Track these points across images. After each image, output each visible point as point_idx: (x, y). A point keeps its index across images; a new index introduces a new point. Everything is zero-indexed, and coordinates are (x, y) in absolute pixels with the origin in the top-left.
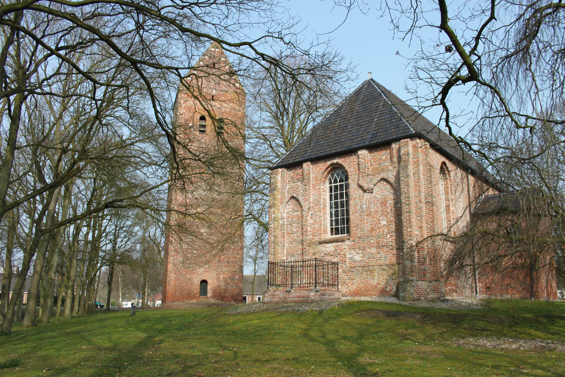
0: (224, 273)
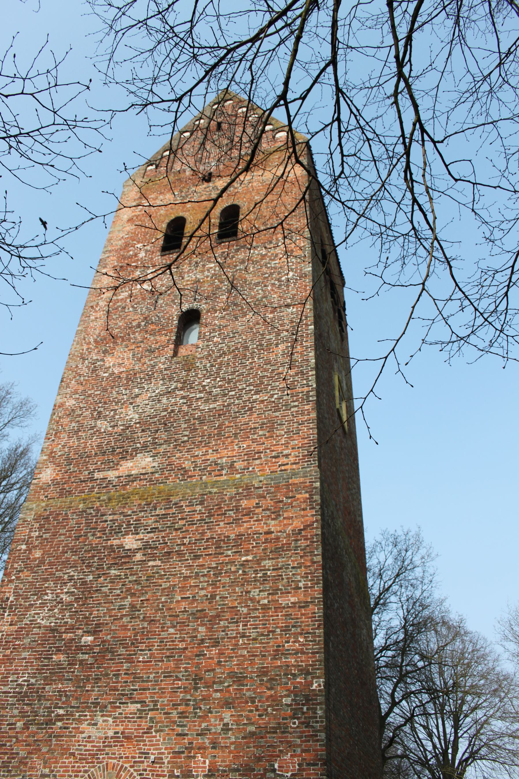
0: (215, 745)
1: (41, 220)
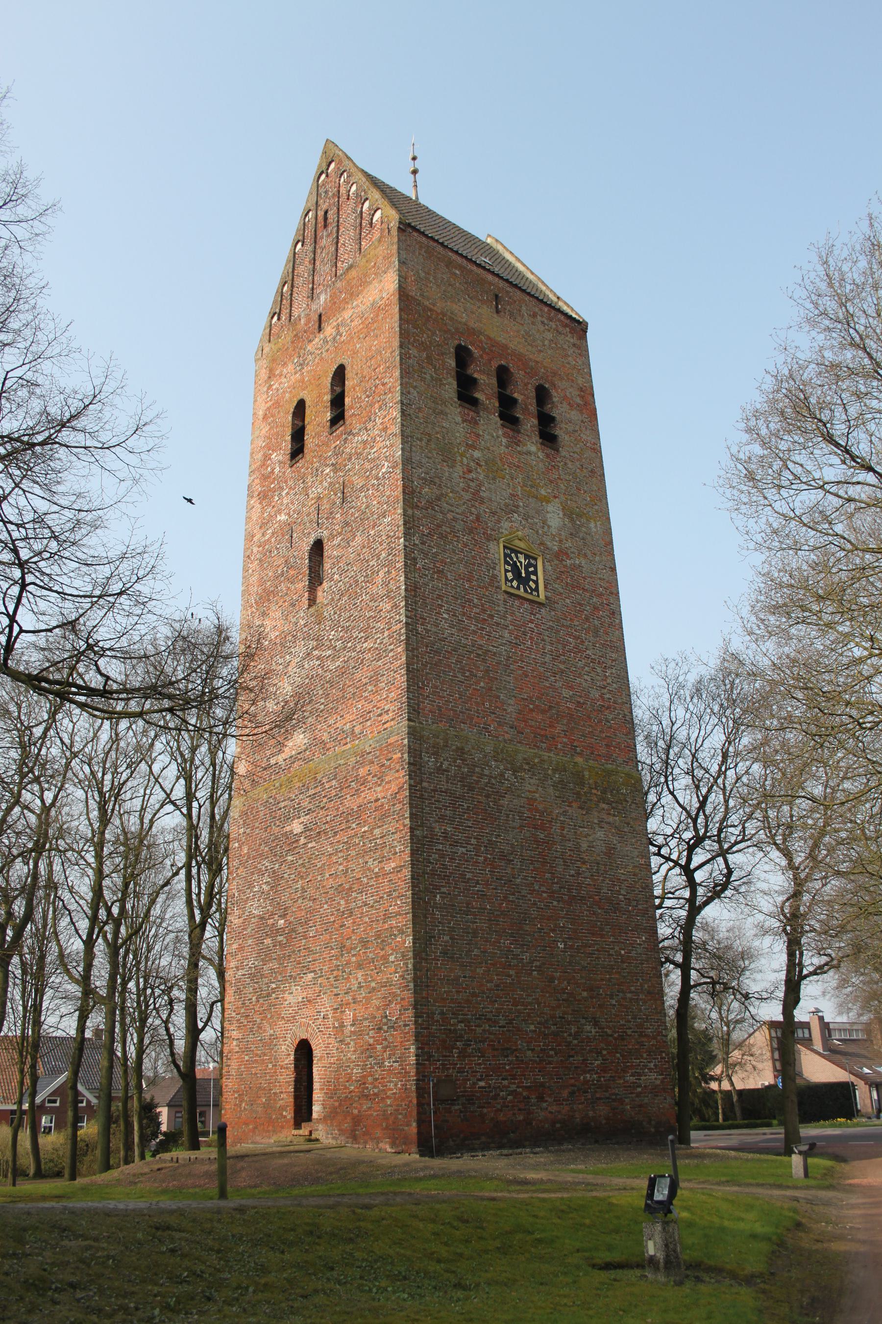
1: (340, 374)
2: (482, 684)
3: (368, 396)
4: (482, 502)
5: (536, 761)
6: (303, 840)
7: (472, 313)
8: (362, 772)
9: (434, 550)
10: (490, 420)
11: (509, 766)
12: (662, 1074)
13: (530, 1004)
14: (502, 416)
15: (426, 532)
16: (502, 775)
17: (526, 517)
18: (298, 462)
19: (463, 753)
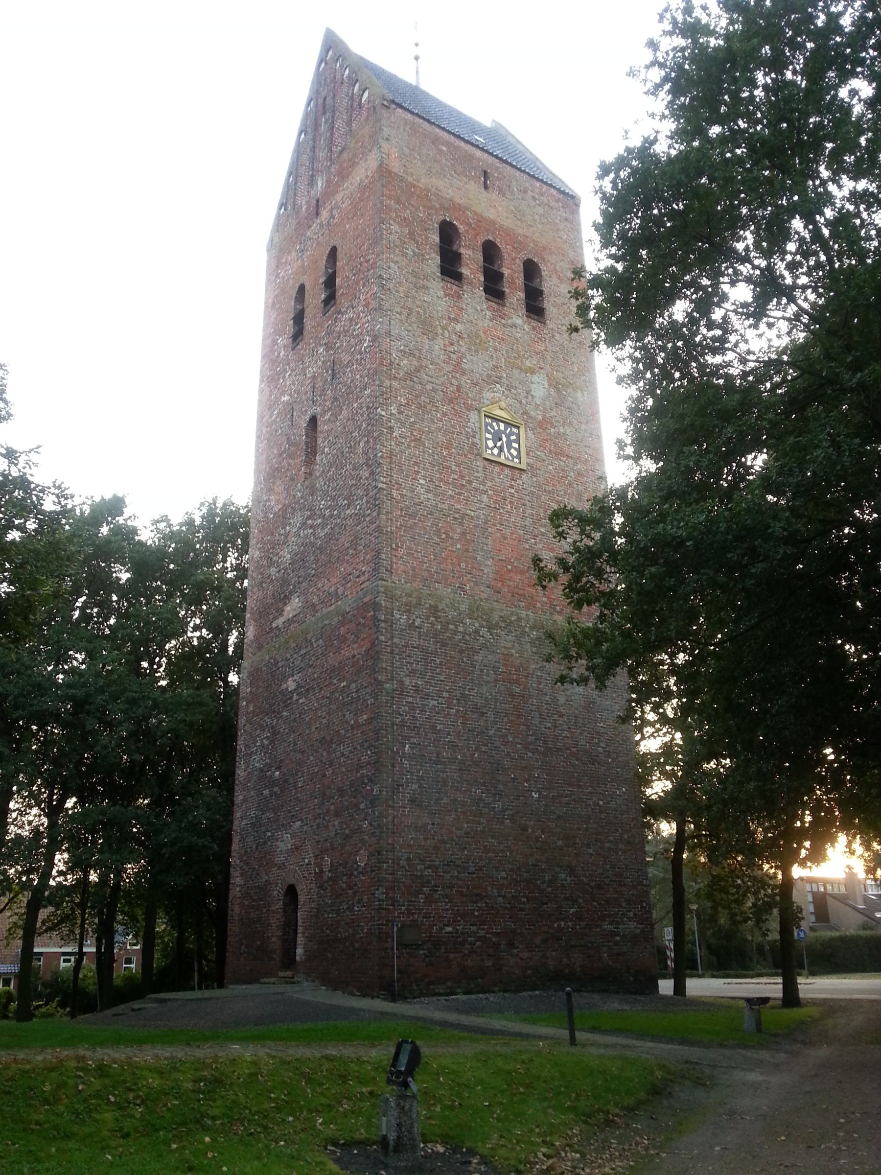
2: (459, 546)
3: (354, 275)
4: (463, 373)
5: (513, 618)
6: (295, 697)
7: (459, 189)
8: (342, 631)
9: (412, 420)
10: (474, 293)
11: (484, 623)
12: (642, 924)
13: (502, 851)
14: (487, 290)
15: (404, 401)
16: (477, 632)
17: (509, 388)
18: (298, 344)
19: (437, 611)
